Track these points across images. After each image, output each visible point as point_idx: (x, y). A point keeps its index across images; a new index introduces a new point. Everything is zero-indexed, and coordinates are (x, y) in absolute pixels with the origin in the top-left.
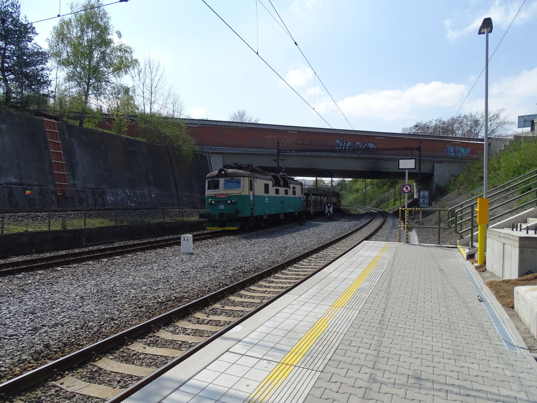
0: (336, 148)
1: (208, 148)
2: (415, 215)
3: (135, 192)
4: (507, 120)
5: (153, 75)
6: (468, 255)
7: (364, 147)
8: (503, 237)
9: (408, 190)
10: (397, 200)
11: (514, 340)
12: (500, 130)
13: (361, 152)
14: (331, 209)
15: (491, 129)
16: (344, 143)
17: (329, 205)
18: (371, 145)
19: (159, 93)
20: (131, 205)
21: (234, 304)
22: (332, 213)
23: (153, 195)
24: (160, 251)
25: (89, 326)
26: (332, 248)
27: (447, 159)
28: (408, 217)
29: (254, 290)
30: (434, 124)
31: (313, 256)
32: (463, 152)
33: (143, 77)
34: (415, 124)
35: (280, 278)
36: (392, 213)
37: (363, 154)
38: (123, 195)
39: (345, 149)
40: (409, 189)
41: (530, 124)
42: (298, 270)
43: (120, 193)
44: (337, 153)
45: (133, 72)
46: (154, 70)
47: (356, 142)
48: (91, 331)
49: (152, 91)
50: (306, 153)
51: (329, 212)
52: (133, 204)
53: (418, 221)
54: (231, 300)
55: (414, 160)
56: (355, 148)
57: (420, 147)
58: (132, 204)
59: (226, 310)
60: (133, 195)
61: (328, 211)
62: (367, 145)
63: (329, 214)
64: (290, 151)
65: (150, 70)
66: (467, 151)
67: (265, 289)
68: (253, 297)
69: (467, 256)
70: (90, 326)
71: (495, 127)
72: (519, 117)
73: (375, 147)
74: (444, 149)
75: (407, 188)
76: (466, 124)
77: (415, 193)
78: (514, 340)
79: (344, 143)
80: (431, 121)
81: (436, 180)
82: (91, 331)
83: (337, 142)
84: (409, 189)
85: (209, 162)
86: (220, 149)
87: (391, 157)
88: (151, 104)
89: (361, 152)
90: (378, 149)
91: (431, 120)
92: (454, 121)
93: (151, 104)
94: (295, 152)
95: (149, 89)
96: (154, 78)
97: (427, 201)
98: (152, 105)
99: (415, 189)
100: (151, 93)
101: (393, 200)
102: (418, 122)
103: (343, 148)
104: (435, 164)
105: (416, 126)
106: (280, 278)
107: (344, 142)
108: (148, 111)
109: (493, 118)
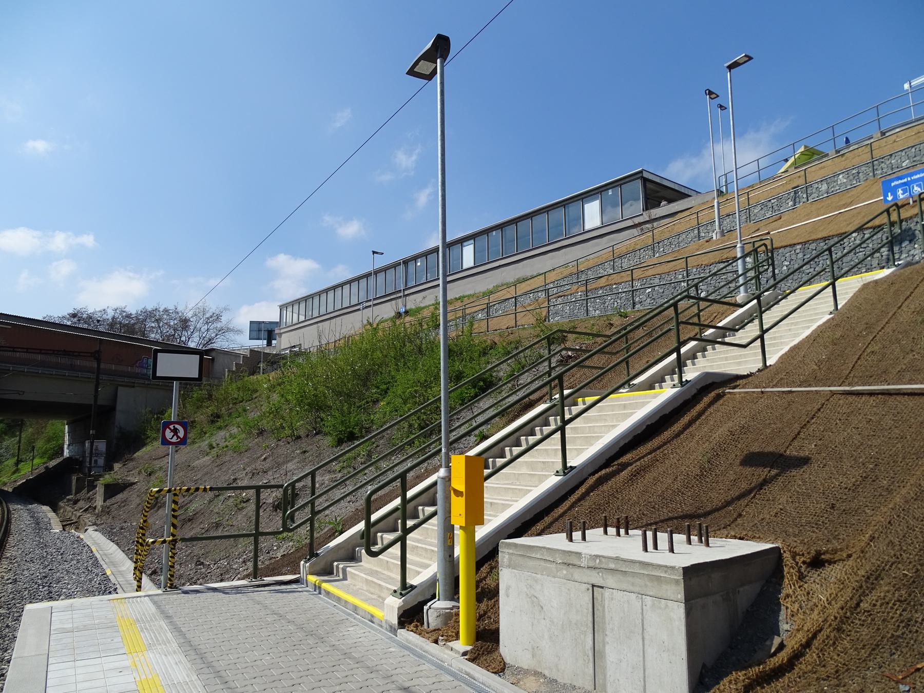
2: (78, 491)
4: (231, 326)
6: (402, 612)
9: (178, 437)
10: (21, 461)
12: (219, 340)
27: (142, 381)
30: (110, 316)
34: (71, 311)
36: (10, 490)
40: (181, 434)
53: (90, 507)
57: (98, 352)
69: (399, 618)
71: (213, 335)
72: (251, 322)
74: (137, 361)
75: (175, 431)
76: (166, 323)
77: (66, 446)
80: (104, 310)
81: (120, 418)
84: (181, 434)
91: (106, 308)
92: (149, 315)
97: (101, 462)
99: (67, 438)
101: (12, 461)
102: (78, 307)
104: (120, 388)
105: (74, 316)
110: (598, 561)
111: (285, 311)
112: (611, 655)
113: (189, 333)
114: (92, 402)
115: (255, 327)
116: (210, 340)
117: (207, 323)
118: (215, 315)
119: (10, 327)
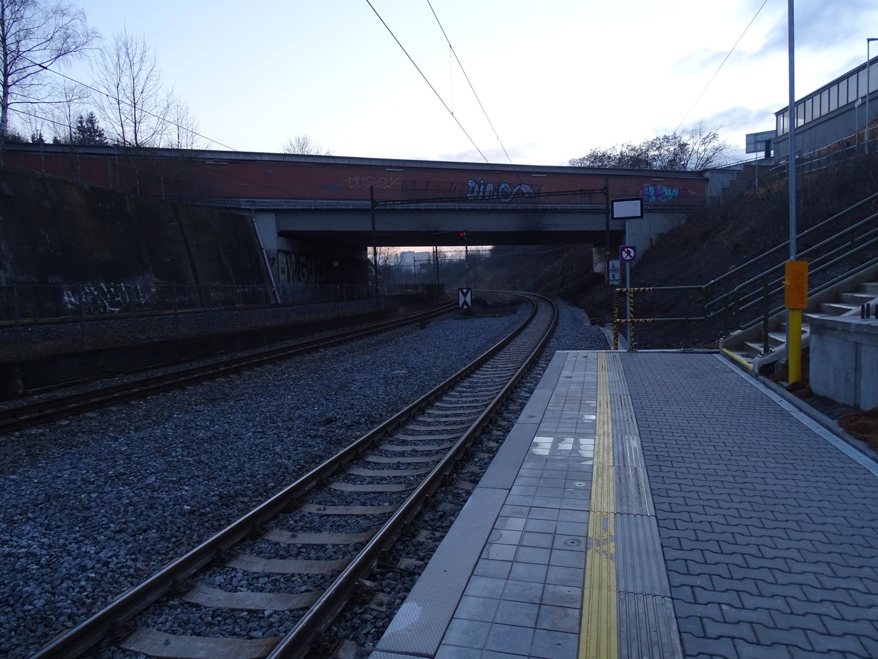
0: (469, 195)
1: (249, 201)
3: (118, 285)
5: (136, 69)
6: (761, 365)
7: (515, 191)
8: (855, 332)
9: (630, 256)
11: (623, 445)
13: (509, 200)
14: (468, 299)
15: (706, 157)
16: (482, 186)
17: (465, 291)
18: (526, 189)
19: (150, 102)
20: (113, 309)
21: (346, 500)
22: (470, 305)
23: (153, 290)
24: (177, 394)
25: (25, 595)
26: (491, 366)
28: (632, 305)
29: (376, 463)
31: (465, 384)
32: (669, 194)
33: (115, 73)
35: (419, 433)
37: (513, 203)
38: (96, 293)
39: (483, 196)
40: (632, 254)
41: (763, 145)
42: (444, 412)
43: (89, 289)
44: (472, 203)
45: (91, 53)
46: (136, 60)
47: (501, 184)
48: (30, 607)
49: (136, 100)
50: (419, 204)
51: (465, 303)
52: (115, 308)
54: (335, 490)
55: (640, 201)
56: (500, 194)
57: (606, 188)
58: (113, 307)
59: (331, 515)
60: (115, 291)
61: (463, 301)
62: (520, 189)
63: (465, 307)
64: (385, 202)
65: (128, 60)
66: (674, 193)
67: (396, 460)
68: (380, 480)
70: (27, 597)
72: (748, 136)
73: (531, 191)
75: (628, 253)
78: (623, 445)
79: (482, 186)
82: (30, 607)
83: (469, 184)
84: (632, 254)
85: (252, 227)
86: (267, 203)
87: (559, 206)
88: (135, 123)
89: (509, 200)
90: (539, 194)
91: (615, 145)
93: (135, 123)
94: (402, 204)
95: (130, 95)
96: (137, 76)
98: (137, 125)
100: (135, 104)
103: (481, 194)
106: (419, 433)
107: (481, 184)
108: (130, 137)
109: (708, 139)
110: (859, 328)
111: (782, 118)
112: (863, 386)
113: (688, 156)
114: (604, 228)
115: (752, 140)
116: (708, 159)
117: (704, 144)
118: (711, 134)
119: (545, 175)
